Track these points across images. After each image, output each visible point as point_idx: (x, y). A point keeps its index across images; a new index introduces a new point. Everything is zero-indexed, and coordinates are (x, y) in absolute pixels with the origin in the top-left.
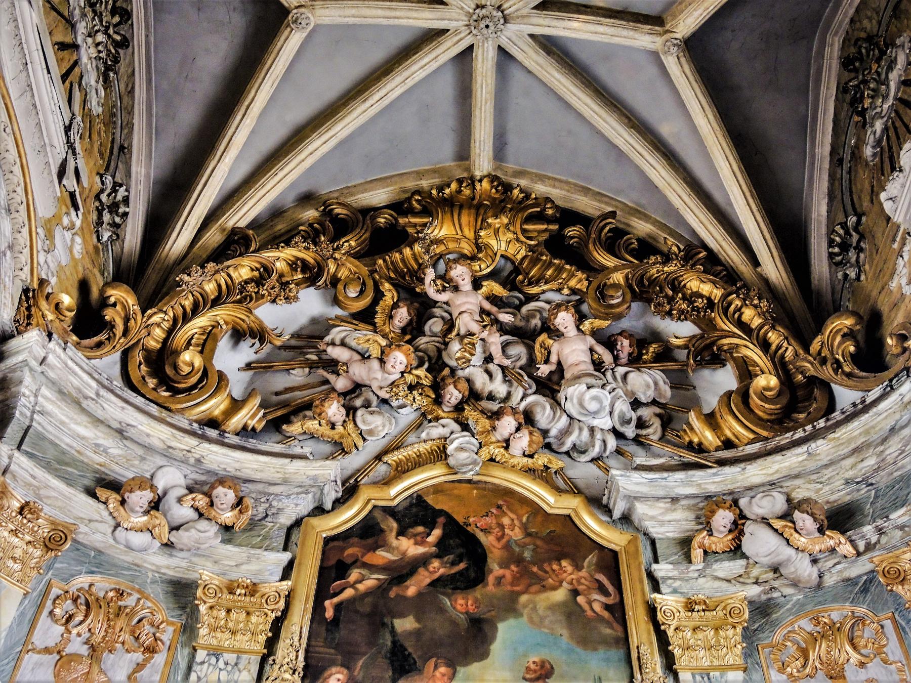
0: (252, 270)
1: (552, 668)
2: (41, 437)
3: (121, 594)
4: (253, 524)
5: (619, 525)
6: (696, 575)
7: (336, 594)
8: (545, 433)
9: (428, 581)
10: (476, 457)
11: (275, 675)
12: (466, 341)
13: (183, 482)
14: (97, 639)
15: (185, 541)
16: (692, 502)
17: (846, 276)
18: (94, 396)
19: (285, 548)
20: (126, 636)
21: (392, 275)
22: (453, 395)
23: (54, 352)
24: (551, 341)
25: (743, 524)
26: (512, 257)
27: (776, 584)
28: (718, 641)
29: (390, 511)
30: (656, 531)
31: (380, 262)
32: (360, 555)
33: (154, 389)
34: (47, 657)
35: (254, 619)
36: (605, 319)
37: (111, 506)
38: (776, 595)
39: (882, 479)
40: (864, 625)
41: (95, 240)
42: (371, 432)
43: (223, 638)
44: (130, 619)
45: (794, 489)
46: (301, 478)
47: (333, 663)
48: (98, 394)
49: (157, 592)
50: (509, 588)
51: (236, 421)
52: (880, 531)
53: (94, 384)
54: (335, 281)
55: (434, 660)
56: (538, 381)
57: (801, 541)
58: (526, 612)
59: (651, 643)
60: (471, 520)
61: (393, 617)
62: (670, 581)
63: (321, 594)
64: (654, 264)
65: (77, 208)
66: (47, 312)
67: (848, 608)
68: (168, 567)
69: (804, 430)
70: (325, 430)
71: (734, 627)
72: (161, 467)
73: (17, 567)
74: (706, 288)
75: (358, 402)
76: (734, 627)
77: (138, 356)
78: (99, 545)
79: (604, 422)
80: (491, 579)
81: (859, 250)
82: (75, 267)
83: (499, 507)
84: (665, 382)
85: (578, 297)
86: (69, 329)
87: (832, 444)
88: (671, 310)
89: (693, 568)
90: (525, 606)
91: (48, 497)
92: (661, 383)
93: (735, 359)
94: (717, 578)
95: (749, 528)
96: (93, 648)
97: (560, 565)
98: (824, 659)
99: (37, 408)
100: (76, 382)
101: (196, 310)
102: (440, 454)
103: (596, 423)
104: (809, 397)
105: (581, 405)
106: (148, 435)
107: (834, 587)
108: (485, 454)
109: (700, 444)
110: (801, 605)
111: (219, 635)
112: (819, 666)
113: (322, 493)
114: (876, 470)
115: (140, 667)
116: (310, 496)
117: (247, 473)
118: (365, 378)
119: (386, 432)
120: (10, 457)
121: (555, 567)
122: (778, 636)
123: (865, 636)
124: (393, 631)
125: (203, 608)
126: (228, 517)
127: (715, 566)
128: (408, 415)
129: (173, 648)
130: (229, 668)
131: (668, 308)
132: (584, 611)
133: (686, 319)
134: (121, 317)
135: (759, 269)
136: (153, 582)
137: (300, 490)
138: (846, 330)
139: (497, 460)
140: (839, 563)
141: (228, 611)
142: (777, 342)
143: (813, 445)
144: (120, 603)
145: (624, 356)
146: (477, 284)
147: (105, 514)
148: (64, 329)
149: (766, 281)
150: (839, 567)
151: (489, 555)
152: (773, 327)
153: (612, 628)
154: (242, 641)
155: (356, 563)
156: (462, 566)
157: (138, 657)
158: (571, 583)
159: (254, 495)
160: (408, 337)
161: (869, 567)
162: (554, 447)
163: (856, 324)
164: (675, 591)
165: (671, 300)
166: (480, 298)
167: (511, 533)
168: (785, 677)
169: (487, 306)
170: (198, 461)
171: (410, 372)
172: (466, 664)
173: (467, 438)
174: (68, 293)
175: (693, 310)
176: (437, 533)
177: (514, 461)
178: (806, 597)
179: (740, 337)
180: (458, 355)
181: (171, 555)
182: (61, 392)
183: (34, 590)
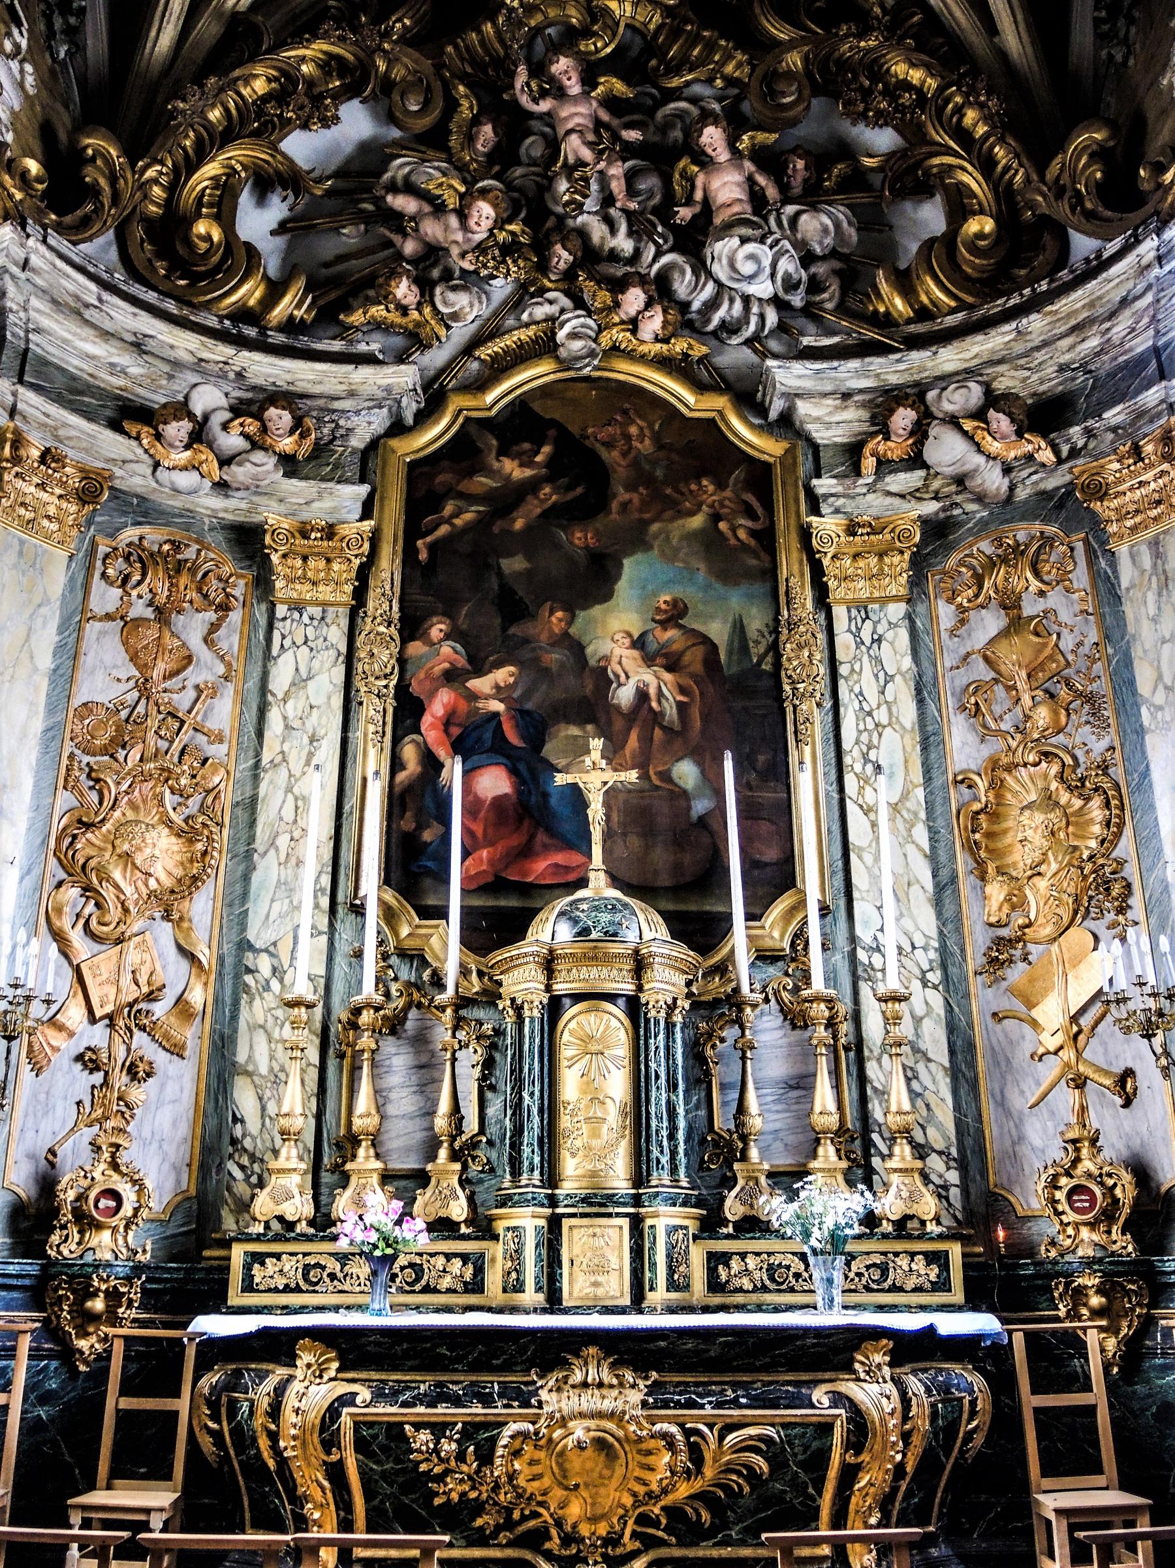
0: (269, 80)
1: (686, 606)
2: (44, 362)
3: (177, 546)
4: (320, 451)
5: (776, 430)
6: (864, 490)
7: (430, 532)
8: (685, 306)
9: (539, 511)
10: (594, 345)
11: (368, 628)
12: (577, 174)
13: (224, 402)
14: (162, 598)
15: (241, 478)
16: (867, 397)
17: (1111, 57)
18: (96, 303)
19: (362, 481)
20: (193, 595)
21: (469, 70)
22: (562, 257)
23: (36, 251)
24: (696, 169)
25: (929, 424)
26: (642, 28)
27: (958, 499)
28: (882, 569)
29: (485, 424)
30: (821, 435)
31: (450, 49)
32: (453, 482)
33: (166, 277)
34: (110, 625)
35: (336, 566)
36: (770, 131)
37: (145, 442)
38: (956, 512)
39: (1104, 365)
40: (1052, 546)
41: (50, 61)
42: (455, 316)
43: (304, 591)
44: (194, 574)
45: (995, 379)
46: (369, 390)
47: (434, 613)
48: (100, 300)
49: (216, 539)
50: (636, 515)
51: (278, 313)
52: (1089, 433)
53: (93, 286)
54: (387, 86)
55: (548, 604)
56: (675, 229)
57: (995, 447)
58: (656, 544)
59: (802, 575)
60: (590, 430)
61: (498, 557)
62: (832, 499)
63: (412, 530)
64: (847, 36)
65: (19, 25)
66: (13, 190)
67: (1037, 527)
68: (226, 510)
69: (1021, 295)
70: (394, 317)
71: (902, 552)
72: (196, 385)
73: (54, 526)
74: (916, 76)
75: (436, 273)
76: (902, 552)
77: (139, 232)
78: (139, 490)
79: (763, 289)
80: (615, 506)
81: (1131, 21)
82: (32, 107)
83: (625, 412)
84: (850, 223)
85: (736, 91)
86: (43, 205)
87: (1049, 319)
88: (866, 110)
89: (861, 481)
90: (656, 537)
91: (69, 438)
92: (845, 225)
93: (946, 189)
94: (889, 494)
95: (935, 430)
96: (159, 610)
97: (700, 484)
98: (1000, 587)
99: (31, 326)
100: (71, 287)
101: (201, 155)
102: (545, 346)
103: (752, 289)
104: (1037, 247)
105: (732, 265)
106: (172, 347)
107: (1026, 502)
108: (605, 340)
109: (887, 313)
110: (984, 524)
111: (298, 587)
112: (993, 595)
113: (399, 406)
114: (1097, 354)
115: (214, 627)
116: (385, 410)
117: (301, 387)
118: (441, 239)
119: (475, 314)
120: (14, 394)
121: (693, 487)
122: (952, 561)
123: (1052, 559)
124: (500, 573)
125: (275, 558)
126: (287, 444)
127: (888, 479)
128: (501, 288)
129: (248, 604)
130: (315, 623)
131: (861, 107)
132: (727, 539)
133: (886, 124)
134: (104, 176)
135: (996, 40)
136: (211, 529)
137: (371, 404)
138: (1095, 147)
139: (623, 346)
140: (1035, 472)
141: (305, 559)
142: (1004, 161)
143: (1025, 321)
144: (179, 557)
145: (797, 184)
146: (589, 81)
147: (140, 451)
148: (38, 208)
149: (1002, 55)
150: (1035, 477)
151: (614, 476)
152: (1002, 140)
153: (758, 557)
154: (325, 592)
155: (450, 492)
156: (579, 490)
157: (211, 616)
158: (712, 506)
159: (314, 414)
160: (497, 168)
161: (1068, 478)
162: (697, 325)
163: (1110, 138)
164: (837, 511)
165: (866, 94)
166: (595, 104)
167: (639, 446)
168: (953, 607)
169: (605, 116)
170: (240, 375)
171: (502, 229)
172: (585, 608)
173: (582, 320)
174: (33, 157)
175: (896, 110)
176: (546, 449)
177: (643, 349)
178: (991, 514)
179: (956, 155)
180: (566, 198)
181: (227, 496)
182: (54, 301)
183: (78, 550)
